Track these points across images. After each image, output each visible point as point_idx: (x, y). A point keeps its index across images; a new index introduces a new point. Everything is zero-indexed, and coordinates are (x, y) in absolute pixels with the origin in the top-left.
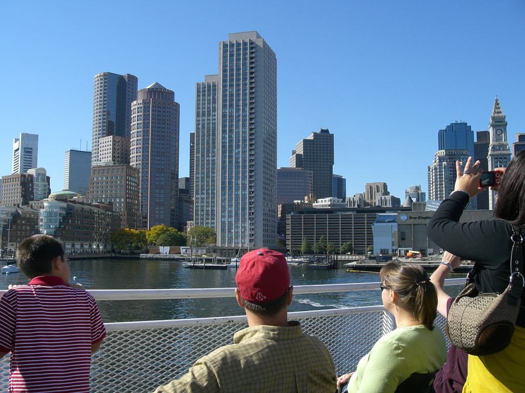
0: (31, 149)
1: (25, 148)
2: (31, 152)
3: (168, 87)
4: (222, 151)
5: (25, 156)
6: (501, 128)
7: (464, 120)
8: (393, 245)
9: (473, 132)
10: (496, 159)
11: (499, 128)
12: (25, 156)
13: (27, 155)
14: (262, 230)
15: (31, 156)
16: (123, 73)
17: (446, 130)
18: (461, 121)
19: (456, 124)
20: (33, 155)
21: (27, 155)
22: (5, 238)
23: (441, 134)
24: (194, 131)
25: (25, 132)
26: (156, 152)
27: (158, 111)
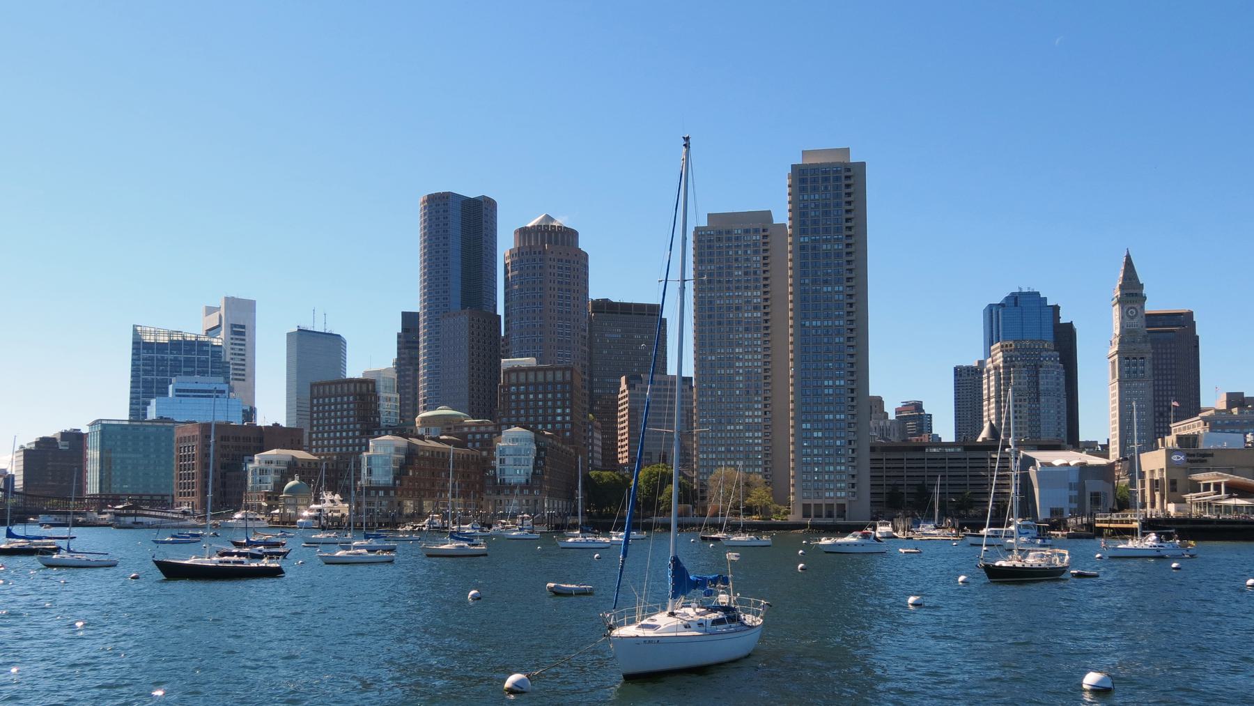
0: (243, 327)
1: (233, 326)
2: (243, 334)
3: (561, 220)
4: (803, 334)
5: (232, 341)
6: (1135, 306)
7: (1025, 285)
8: (1070, 501)
9: (500, 316)
10: (1127, 358)
11: (1133, 306)
12: (232, 341)
13: (237, 339)
14: (868, 461)
15: (244, 340)
16: (472, 194)
17: (1001, 305)
18: (1029, 288)
19: (1020, 293)
20: (247, 338)
21: (237, 339)
22: (913, 407)
23: (993, 312)
24: (415, 304)
25: (230, 295)
26: (556, 340)
27: (559, 268)
